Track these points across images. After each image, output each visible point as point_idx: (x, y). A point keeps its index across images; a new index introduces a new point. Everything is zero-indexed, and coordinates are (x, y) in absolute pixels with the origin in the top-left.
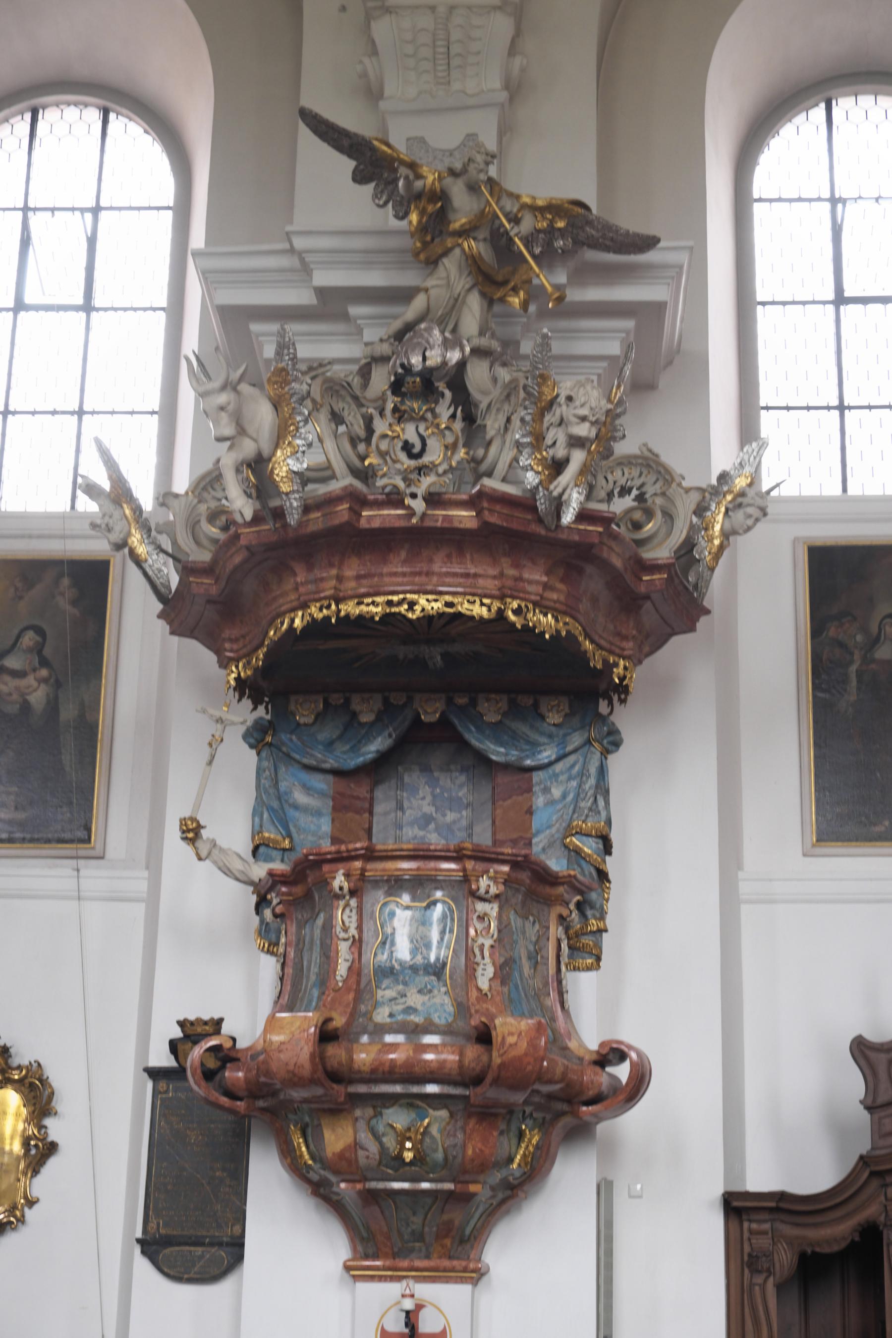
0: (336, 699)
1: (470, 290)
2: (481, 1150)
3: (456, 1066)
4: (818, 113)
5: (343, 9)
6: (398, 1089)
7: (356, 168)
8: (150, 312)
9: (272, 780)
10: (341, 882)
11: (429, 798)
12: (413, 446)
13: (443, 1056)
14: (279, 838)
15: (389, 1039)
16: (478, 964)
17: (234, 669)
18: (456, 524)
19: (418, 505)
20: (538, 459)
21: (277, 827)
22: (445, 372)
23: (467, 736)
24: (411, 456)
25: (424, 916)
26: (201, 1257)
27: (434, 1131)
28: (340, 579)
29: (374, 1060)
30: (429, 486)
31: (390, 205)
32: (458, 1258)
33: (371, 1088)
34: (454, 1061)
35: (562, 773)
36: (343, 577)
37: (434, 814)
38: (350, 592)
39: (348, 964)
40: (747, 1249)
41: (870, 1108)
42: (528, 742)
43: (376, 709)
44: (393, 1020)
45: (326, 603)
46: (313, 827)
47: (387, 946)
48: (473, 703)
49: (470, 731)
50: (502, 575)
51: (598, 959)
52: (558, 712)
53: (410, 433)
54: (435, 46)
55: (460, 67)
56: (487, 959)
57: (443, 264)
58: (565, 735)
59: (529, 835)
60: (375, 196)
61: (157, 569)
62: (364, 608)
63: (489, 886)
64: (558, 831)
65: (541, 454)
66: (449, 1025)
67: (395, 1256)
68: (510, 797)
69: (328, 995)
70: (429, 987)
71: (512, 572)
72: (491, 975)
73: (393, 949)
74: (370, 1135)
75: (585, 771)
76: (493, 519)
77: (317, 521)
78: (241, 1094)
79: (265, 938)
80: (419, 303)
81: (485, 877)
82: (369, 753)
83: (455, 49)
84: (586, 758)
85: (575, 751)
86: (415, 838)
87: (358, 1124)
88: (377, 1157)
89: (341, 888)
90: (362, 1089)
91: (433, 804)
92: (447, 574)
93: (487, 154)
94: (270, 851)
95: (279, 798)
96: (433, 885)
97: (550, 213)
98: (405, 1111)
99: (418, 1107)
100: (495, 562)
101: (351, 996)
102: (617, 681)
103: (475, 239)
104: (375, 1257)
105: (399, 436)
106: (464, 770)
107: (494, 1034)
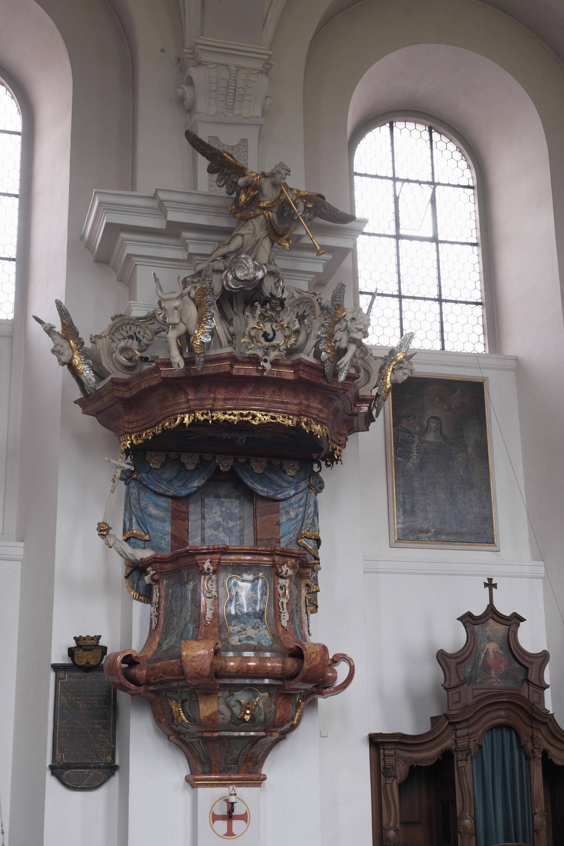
0: (173, 455)
2: (283, 714)
3: (280, 669)
4: (386, 128)
5: (163, 51)
6: (248, 681)
7: (210, 165)
11: (218, 514)
12: (269, 335)
13: (274, 664)
15: (246, 654)
16: (281, 613)
17: (129, 438)
18: (284, 377)
19: (267, 366)
20: (329, 346)
21: (141, 528)
22: (254, 283)
23: (245, 480)
24: (267, 340)
26: (88, 775)
27: (261, 704)
28: (215, 399)
29: (238, 666)
30: (275, 356)
31: (225, 186)
32: (253, 773)
33: (232, 681)
34: (279, 667)
35: (295, 503)
36: (216, 398)
37: (222, 522)
39: (212, 612)
40: (382, 765)
41: (446, 689)
42: (278, 485)
44: (241, 643)
45: (205, 412)
46: (160, 528)
48: (248, 462)
49: (247, 478)
50: (300, 403)
51: (317, 607)
52: (294, 470)
56: (285, 611)
57: (252, 221)
58: (298, 483)
59: (278, 537)
60: (218, 181)
62: (227, 416)
63: (287, 570)
64: (293, 536)
65: (331, 344)
66: (271, 646)
67: (220, 773)
68: (266, 515)
69: (202, 629)
71: (305, 402)
72: (288, 619)
74: (226, 707)
75: (307, 503)
76: (304, 376)
77: (211, 369)
78: (142, 682)
79: (136, 592)
80: (238, 241)
82: (193, 488)
85: (302, 491)
86: (212, 535)
87: (219, 700)
89: (208, 569)
90: (227, 681)
91: (221, 516)
93: (287, 170)
94: (137, 541)
95: (141, 510)
96: (257, 569)
97: (305, 200)
98: (247, 693)
99: (254, 691)
101: (216, 630)
102: (336, 457)
103: (271, 211)
104: (210, 773)
106: (238, 498)
107: (305, 652)
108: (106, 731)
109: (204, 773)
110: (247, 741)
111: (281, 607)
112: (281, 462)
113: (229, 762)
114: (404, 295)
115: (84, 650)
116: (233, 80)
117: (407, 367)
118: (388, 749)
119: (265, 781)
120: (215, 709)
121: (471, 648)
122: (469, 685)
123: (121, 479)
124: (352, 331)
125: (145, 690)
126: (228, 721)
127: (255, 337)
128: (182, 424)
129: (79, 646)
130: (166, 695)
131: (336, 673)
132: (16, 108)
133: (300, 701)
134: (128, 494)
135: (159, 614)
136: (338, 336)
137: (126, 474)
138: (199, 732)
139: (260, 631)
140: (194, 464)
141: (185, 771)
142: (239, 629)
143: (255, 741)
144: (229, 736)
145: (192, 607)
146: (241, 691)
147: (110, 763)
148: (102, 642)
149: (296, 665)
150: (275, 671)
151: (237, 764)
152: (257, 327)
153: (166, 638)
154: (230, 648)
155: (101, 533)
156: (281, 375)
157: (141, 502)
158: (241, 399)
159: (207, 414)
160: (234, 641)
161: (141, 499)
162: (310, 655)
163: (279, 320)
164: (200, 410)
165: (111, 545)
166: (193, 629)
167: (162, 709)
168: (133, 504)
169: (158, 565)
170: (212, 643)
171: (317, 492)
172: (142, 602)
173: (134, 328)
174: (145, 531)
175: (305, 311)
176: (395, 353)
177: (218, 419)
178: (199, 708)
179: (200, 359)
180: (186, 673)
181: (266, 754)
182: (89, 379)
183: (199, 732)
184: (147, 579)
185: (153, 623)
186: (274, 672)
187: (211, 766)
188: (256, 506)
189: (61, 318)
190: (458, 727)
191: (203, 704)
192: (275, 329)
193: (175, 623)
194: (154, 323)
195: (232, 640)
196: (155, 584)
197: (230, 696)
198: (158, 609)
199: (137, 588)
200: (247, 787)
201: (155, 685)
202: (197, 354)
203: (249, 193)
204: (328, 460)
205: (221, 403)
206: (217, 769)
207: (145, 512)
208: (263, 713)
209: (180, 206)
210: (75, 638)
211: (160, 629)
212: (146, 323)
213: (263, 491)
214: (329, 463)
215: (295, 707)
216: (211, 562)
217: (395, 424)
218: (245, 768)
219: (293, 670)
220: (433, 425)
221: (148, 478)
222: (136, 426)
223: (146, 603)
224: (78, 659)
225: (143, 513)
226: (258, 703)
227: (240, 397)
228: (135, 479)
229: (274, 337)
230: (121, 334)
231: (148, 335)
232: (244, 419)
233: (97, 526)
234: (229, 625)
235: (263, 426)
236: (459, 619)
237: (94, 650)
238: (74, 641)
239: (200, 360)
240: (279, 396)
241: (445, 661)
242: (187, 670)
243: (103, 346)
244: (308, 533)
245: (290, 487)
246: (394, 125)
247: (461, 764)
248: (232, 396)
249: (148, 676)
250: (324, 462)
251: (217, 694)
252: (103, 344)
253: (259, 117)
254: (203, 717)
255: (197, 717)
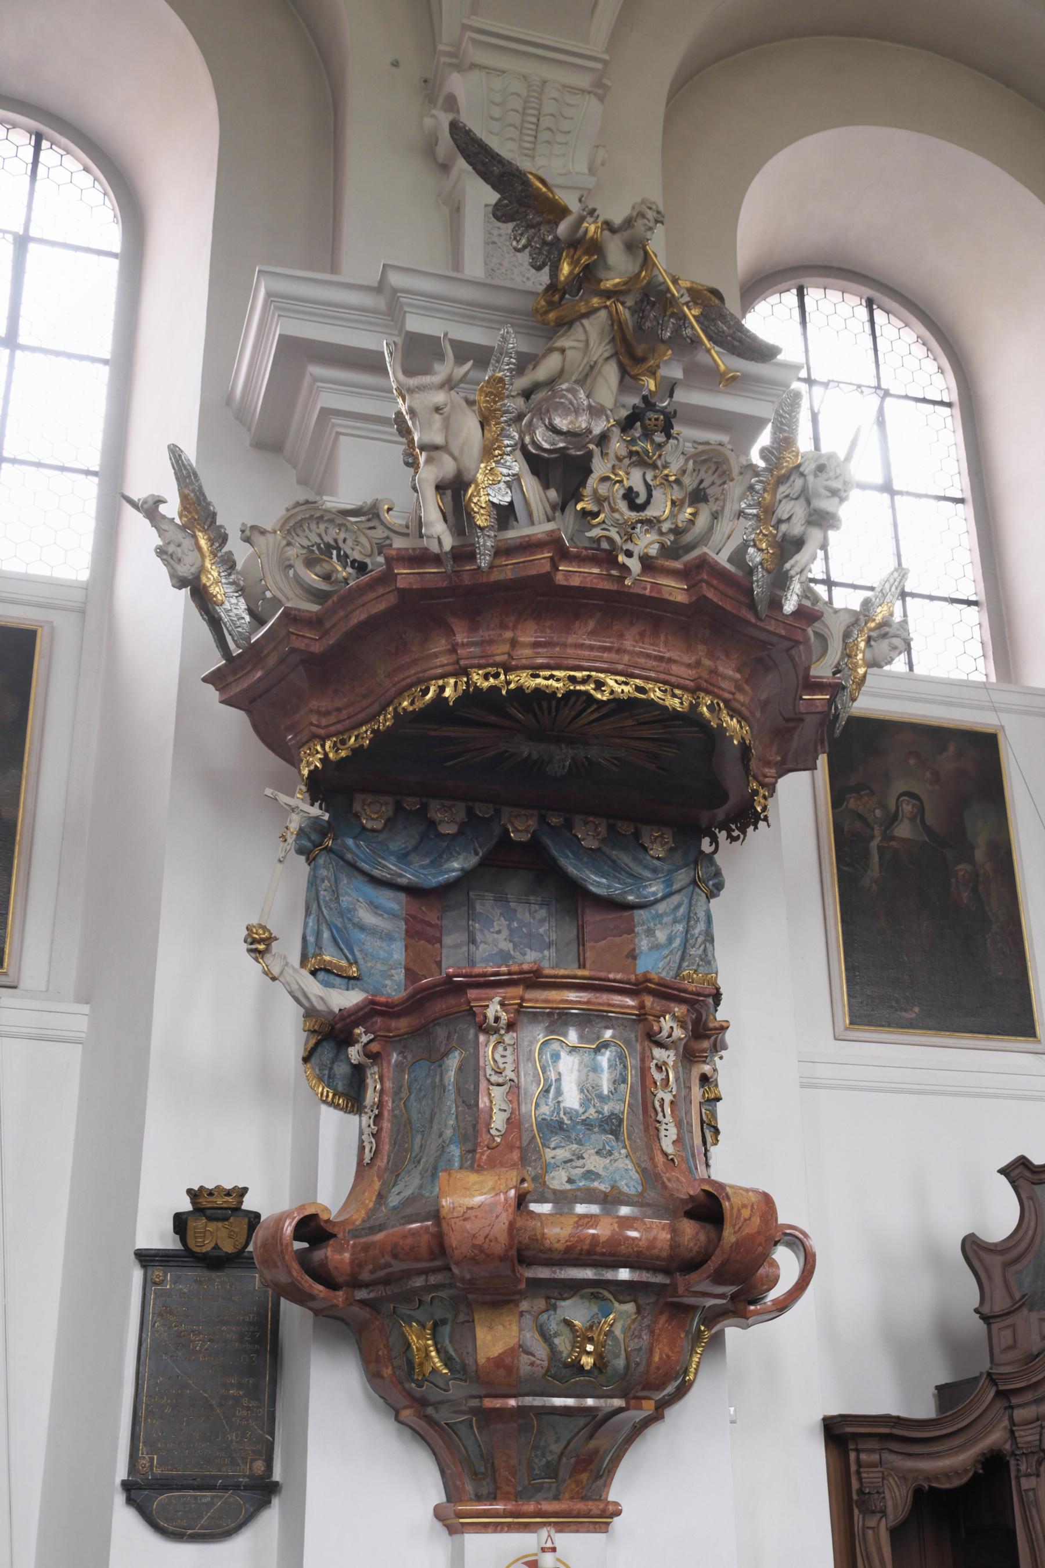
0: (411, 803)
1: (607, 359)
2: (668, 1356)
3: (666, 1246)
5: (395, 64)
6: (588, 1274)
8: (86, 364)
9: (333, 891)
10: (497, 1011)
11: (505, 933)
12: (638, 495)
14: (344, 963)
16: (659, 1122)
17: (319, 748)
18: (666, 596)
19: (634, 565)
21: (341, 950)
24: (634, 506)
25: (594, 1059)
27: (618, 1331)
28: (514, 643)
29: (571, 1235)
31: (527, 250)
32: (590, 1499)
33: (554, 1272)
35: (666, 914)
36: (517, 641)
37: (512, 952)
38: (524, 661)
39: (505, 1116)
40: (855, 1485)
41: (985, 1318)
42: (631, 875)
43: (458, 820)
44: (574, 1187)
45: (492, 670)
46: (383, 954)
47: (551, 1094)
48: (569, 825)
49: (567, 857)
50: (698, 664)
53: (635, 479)
54: (524, 114)
55: (548, 142)
58: (671, 872)
61: (236, 615)
62: (539, 681)
63: (672, 1028)
65: (768, 529)
66: (641, 1194)
67: (518, 1496)
68: (604, 939)
69: (482, 1154)
70: (608, 1148)
71: (707, 662)
72: (675, 1137)
73: (560, 1099)
74: (537, 1336)
77: (509, 570)
78: (341, 1280)
79: (328, 1086)
81: (667, 1017)
82: (454, 870)
83: (546, 122)
84: (691, 899)
85: (679, 891)
87: (523, 1320)
88: (546, 1364)
89: (497, 1019)
90: (543, 1273)
92: (640, 654)
96: (603, 1024)
98: (587, 1303)
99: (604, 1299)
100: (690, 648)
101: (515, 1155)
103: (623, 303)
104: (493, 1498)
105: (621, 482)
107: (726, 1205)
108: (252, 1404)
109: (479, 1498)
110: (582, 1422)
111: (659, 1109)
112: (636, 829)
113: (537, 1472)
114: (836, 580)
115: (211, 1219)
116: (534, 97)
117: (899, 632)
118: (866, 1451)
119: (618, 1517)
120: (513, 1342)
121: (1030, 1233)
122: (1031, 1310)
123: (300, 851)
124: (818, 495)
125: (347, 1298)
126: (543, 1371)
127: (606, 499)
128: (439, 698)
129: (199, 1210)
130: (394, 1312)
131: (777, 1267)
132: (112, 213)
133: (702, 1328)
134: (313, 882)
135: (380, 1130)
136: (784, 510)
137: (309, 839)
138: (473, 1397)
139: (616, 1160)
140: (456, 822)
141: (435, 1493)
142: (568, 1155)
143: (596, 1420)
144: (543, 1407)
145: (457, 1107)
146: (574, 1299)
147: (262, 1478)
148: (249, 1203)
149: (702, 1237)
150: (655, 1248)
151: (556, 1478)
152: (613, 477)
153: (395, 1182)
154: (550, 1195)
155: (254, 947)
156: (660, 592)
157: (341, 898)
158: (571, 646)
159: (496, 676)
160: (558, 1180)
161: (341, 891)
162: (739, 1210)
163: (659, 463)
164: (480, 667)
165: (276, 975)
166: (461, 1156)
167: (386, 1346)
168: (324, 901)
169: (379, 1020)
170: (513, 1176)
171: (711, 895)
172: (341, 1109)
173: (333, 531)
174: (350, 957)
175: (702, 481)
176: (872, 605)
177: (522, 686)
178: (474, 1339)
179: (485, 541)
180: (451, 1246)
181: (618, 1456)
182: (236, 615)
183: (473, 1397)
184: (354, 1053)
185: (367, 1150)
186: (653, 1251)
187: (495, 1481)
188: (583, 920)
189: (179, 485)
190: (1014, 1401)
191: (485, 1329)
192: (651, 483)
193: (416, 1147)
194: (374, 528)
195: (553, 1178)
196: (373, 1064)
197: (547, 1310)
198: (378, 1119)
199: (329, 1077)
200: (577, 1531)
201: (371, 1288)
202: (479, 527)
203: (579, 260)
204: (733, 827)
205: (527, 652)
206: (508, 1489)
207: (350, 920)
208: (623, 1352)
209: (433, 304)
210: (190, 1192)
211: (382, 1163)
212: (362, 526)
213: (599, 885)
214: (736, 833)
215: (690, 1341)
216: (502, 1004)
217: (837, 801)
218: (573, 1486)
219: (696, 1249)
220: (907, 808)
221: (358, 846)
222: (335, 720)
223: (350, 1113)
224: (196, 1238)
225: (346, 920)
226: (613, 1329)
227: (571, 640)
228: (329, 850)
229: (648, 502)
230: (307, 537)
231: (363, 546)
232: (578, 688)
233: (246, 932)
234: (544, 1145)
235: (620, 706)
236: (1002, 1171)
237: (232, 1220)
238: (188, 1199)
239: (485, 544)
240: (652, 645)
241: (980, 1260)
242: (454, 1239)
243: (268, 551)
244: (695, 976)
245: (655, 880)
246: (805, 293)
247: (1026, 1484)
248: (552, 637)
249: (357, 1264)
250: (724, 833)
251: (517, 1306)
252: (267, 546)
253: (583, 174)
254: (484, 1361)
255: (470, 1361)
